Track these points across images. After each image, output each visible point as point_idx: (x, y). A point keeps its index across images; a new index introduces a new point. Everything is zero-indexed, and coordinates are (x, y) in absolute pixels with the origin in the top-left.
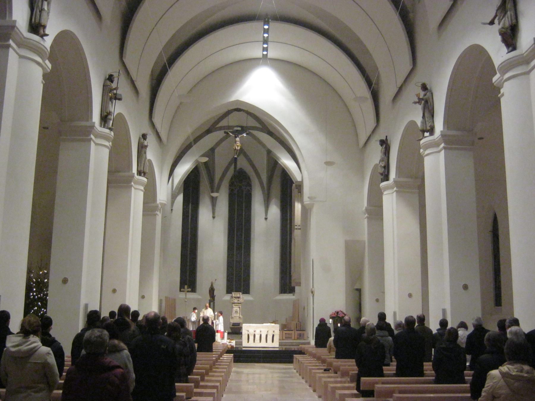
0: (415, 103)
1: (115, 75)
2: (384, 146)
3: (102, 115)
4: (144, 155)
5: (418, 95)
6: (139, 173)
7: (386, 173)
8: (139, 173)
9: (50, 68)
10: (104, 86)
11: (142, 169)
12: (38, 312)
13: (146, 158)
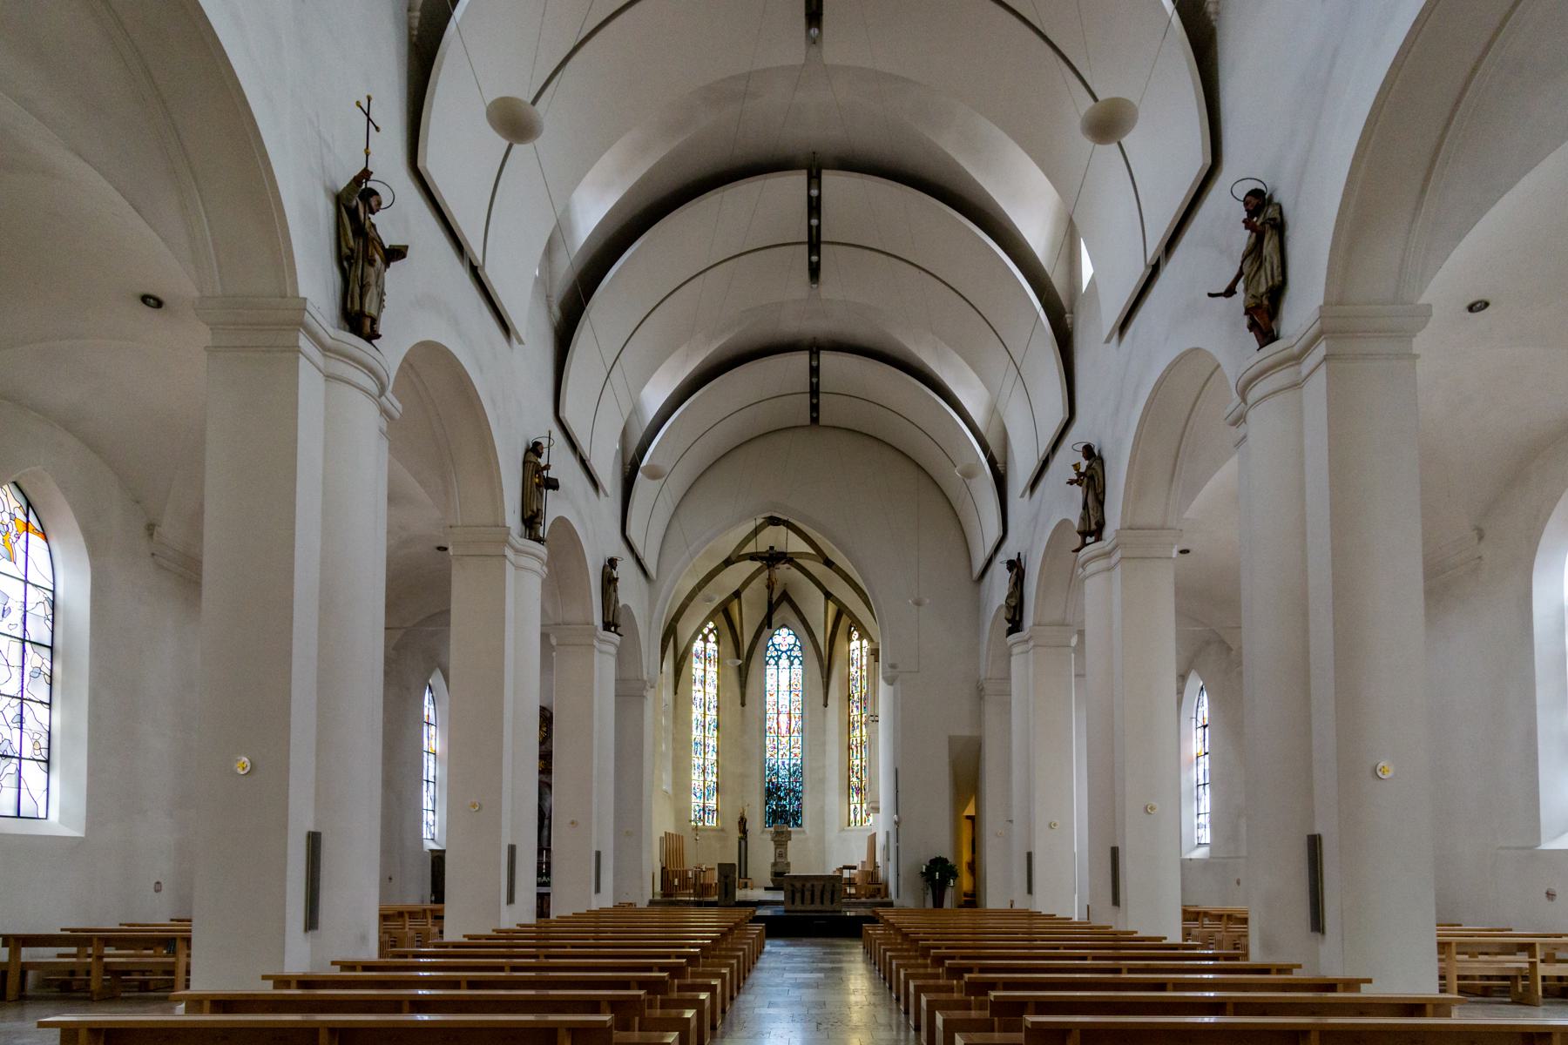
0: (1071, 482)
1: (545, 443)
2: (1015, 571)
3: (525, 517)
4: (613, 594)
5: (1076, 467)
6: (607, 626)
7: (1017, 618)
8: (607, 626)
9: (400, 409)
10: (525, 463)
11: (611, 619)
12: (938, 869)
13: (617, 601)
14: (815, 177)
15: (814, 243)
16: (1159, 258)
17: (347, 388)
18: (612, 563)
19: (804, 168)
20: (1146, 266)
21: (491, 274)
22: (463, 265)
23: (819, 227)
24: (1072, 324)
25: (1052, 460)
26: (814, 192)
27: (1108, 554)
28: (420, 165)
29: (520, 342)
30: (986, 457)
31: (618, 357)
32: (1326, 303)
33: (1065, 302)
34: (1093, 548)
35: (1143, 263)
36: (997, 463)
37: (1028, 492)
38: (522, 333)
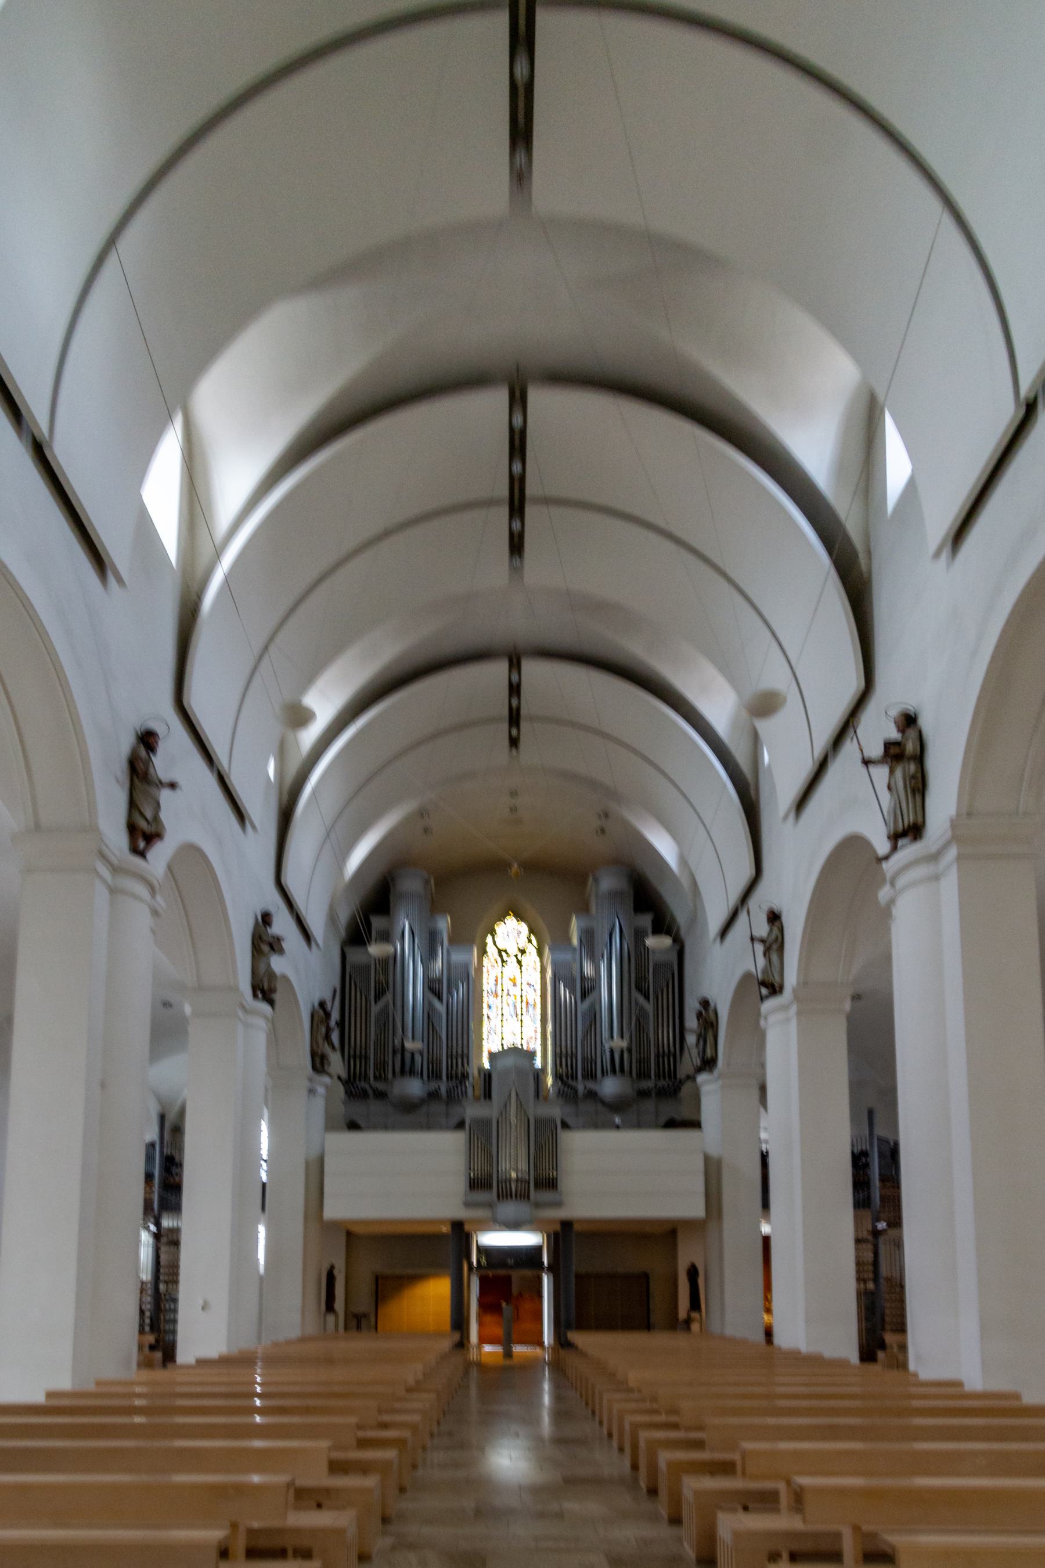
15: (514, 718)
18: (266, 918)
20: (729, 912)
21: (61, 454)
22: (292, 917)
24: (870, 572)
26: (515, 678)
29: (120, 580)
32: (958, 815)
34: (909, 851)
35: (811, 758)
38: (257, 823)
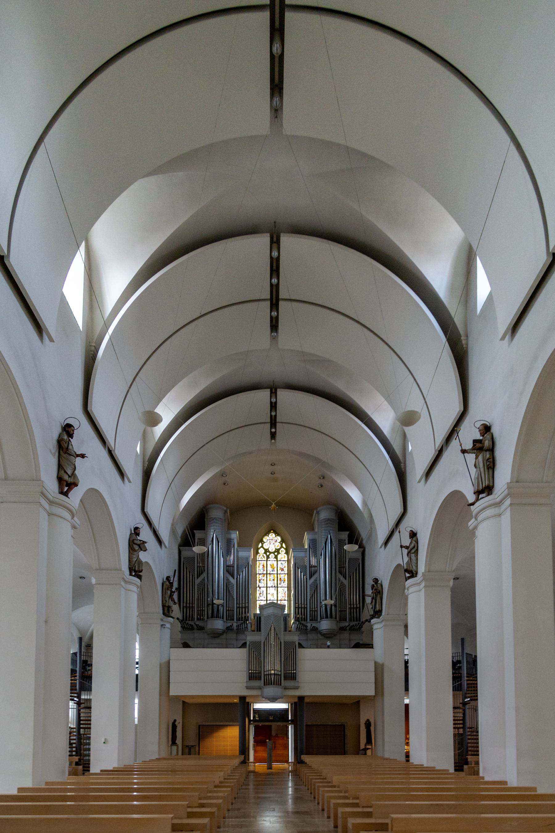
14: (275, 243)
15: (273, 422)
16: (443, 445)
17: (130, 592)
19: (267, 232)
20: (436, 451)
21: (118, 453)
22: (151, 530)
23: (275, 416)
25: (446, 449)
26: (276, 99)
27: (498, 504)
28: (145, 510)
30: (446, 336)
31: (173, 480)
33: (462, 332)
34: (485, 500)
36: (461, 336)
37: (383, 546)
